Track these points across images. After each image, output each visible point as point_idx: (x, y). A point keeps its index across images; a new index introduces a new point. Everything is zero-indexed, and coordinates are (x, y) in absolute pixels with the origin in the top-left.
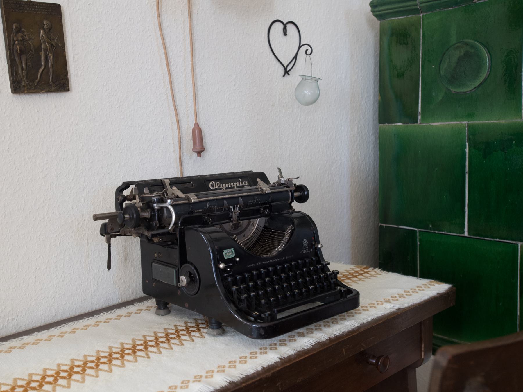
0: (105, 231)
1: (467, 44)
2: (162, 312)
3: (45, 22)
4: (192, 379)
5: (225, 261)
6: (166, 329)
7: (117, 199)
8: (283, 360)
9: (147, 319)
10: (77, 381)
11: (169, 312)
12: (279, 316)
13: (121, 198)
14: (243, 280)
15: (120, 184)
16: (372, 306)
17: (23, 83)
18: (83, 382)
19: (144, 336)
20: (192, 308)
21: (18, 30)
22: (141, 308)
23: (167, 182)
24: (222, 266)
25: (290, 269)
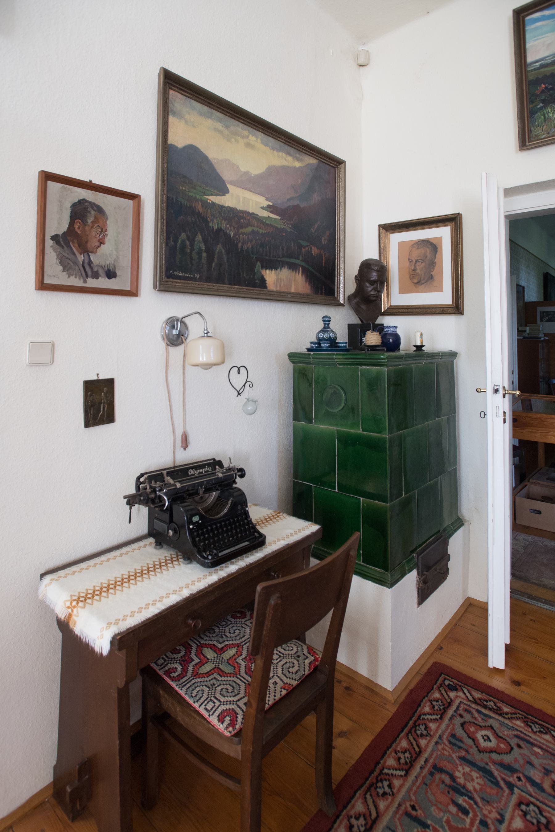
0: (128, 503)
1: (335, 387)
2: (158, 547)
3: (105, 389)
4: (171, 592)
5: (193, 524)
6: (160, 559)
7: (136, 484)
8: (220, 580)
9: (149, 552)
10: (112, 594)
11: (162, 547)
12: (220, 555)
13: (139, 484)
14: (203, 534)
15: (139, 475)
16: (274, 542)
17: (90, 422)
18: (115, 594)
19: (148, 564)
20: (174, 547)
21: (91, 395)
22: (146, 543)
23: (165, 472)
24: (191, 527)
25: (230, 524)
